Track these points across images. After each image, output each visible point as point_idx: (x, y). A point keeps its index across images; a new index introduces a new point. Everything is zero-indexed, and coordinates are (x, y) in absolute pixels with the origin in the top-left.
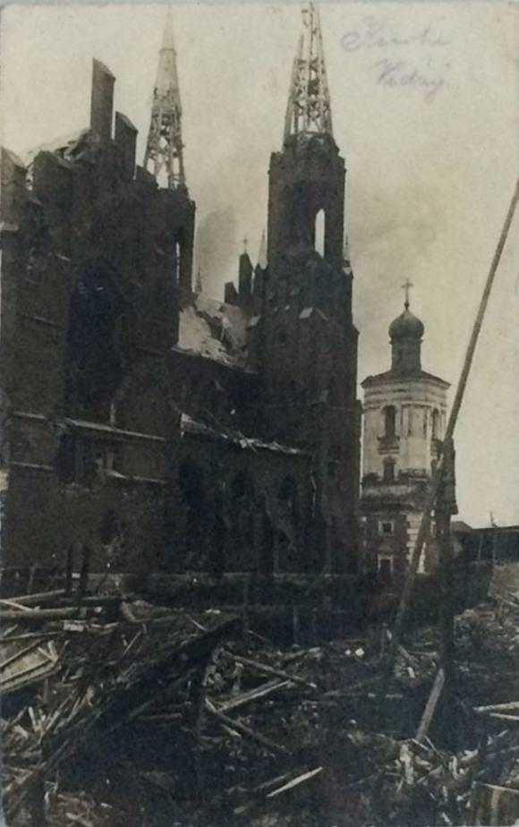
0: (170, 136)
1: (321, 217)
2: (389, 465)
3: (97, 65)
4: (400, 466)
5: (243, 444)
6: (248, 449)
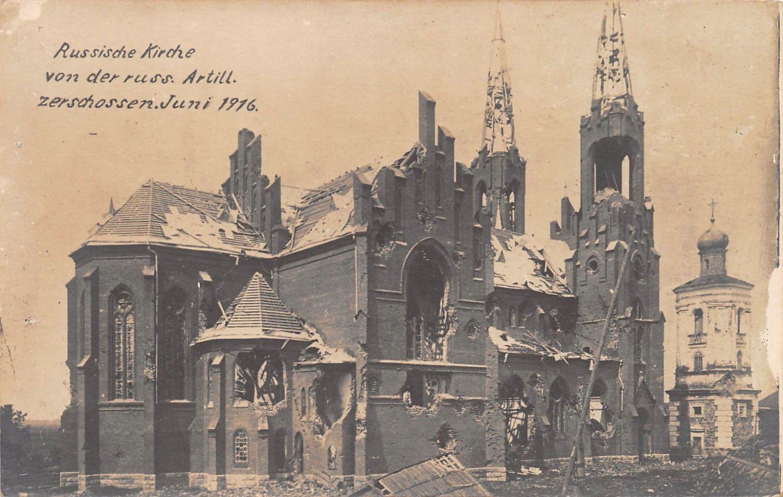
0: (503, 109)
1: (626, 163)
2: (698, 358)
3: (421, 96)
4: (707, 361)
5: (557, 358)
6: (561, 362)
